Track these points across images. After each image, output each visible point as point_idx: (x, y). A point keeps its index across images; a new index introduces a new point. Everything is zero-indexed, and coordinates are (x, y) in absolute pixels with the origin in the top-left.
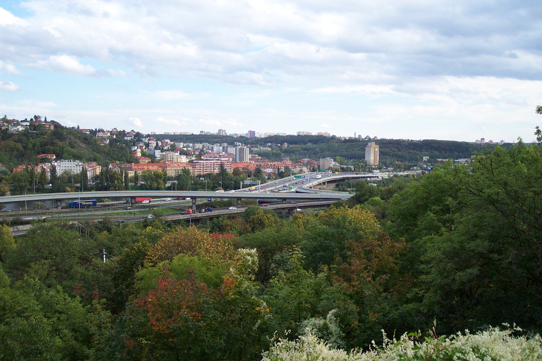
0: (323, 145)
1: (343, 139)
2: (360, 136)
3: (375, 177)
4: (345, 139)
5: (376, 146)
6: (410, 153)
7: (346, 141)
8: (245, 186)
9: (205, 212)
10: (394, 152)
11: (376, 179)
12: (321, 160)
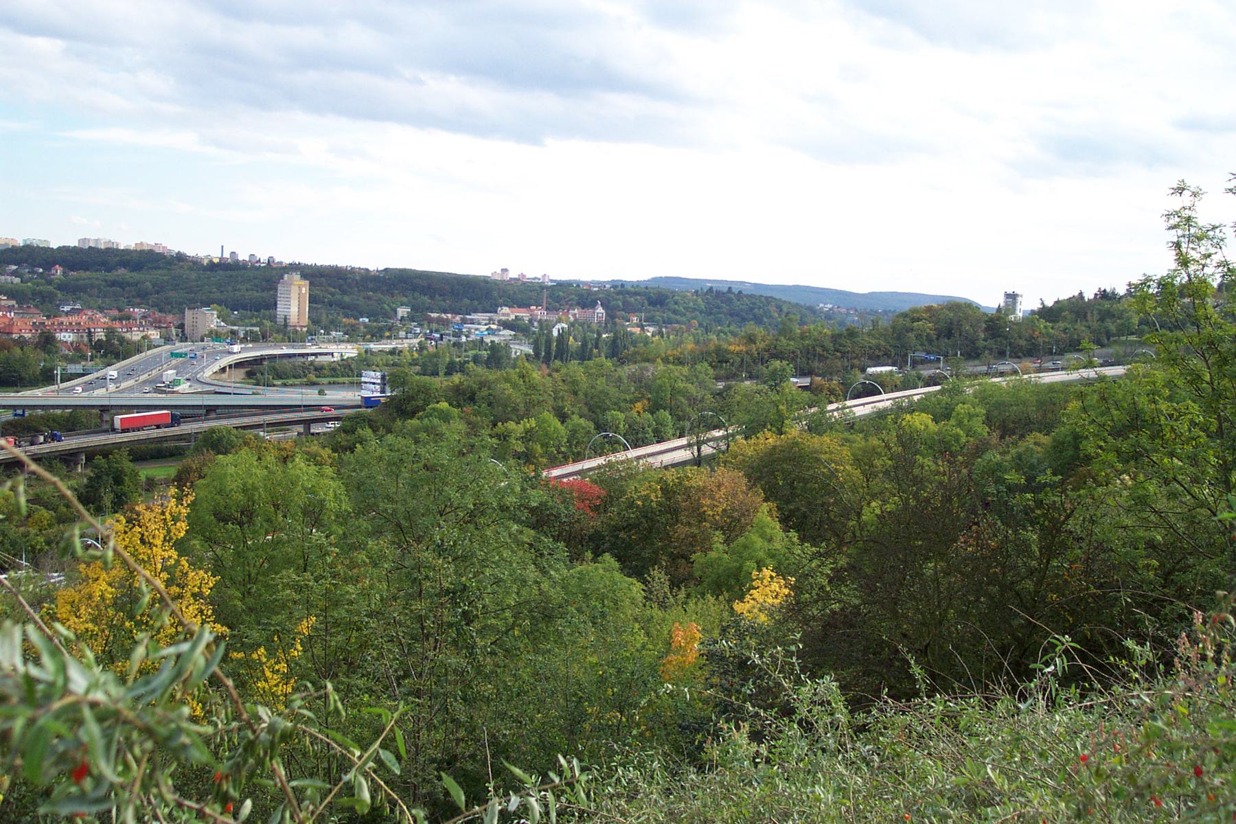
0: (160, 275)
1: (205, 262)
2: (233, 253)
3: (326, 354)
4: (211, 261)
5: (303, 282)
6: (369, 298)
7: (212, 267)
8: (67, 378)
9: (45, 441)
10: (333, 295)
11: (329, 358)
12: (189, 314)
